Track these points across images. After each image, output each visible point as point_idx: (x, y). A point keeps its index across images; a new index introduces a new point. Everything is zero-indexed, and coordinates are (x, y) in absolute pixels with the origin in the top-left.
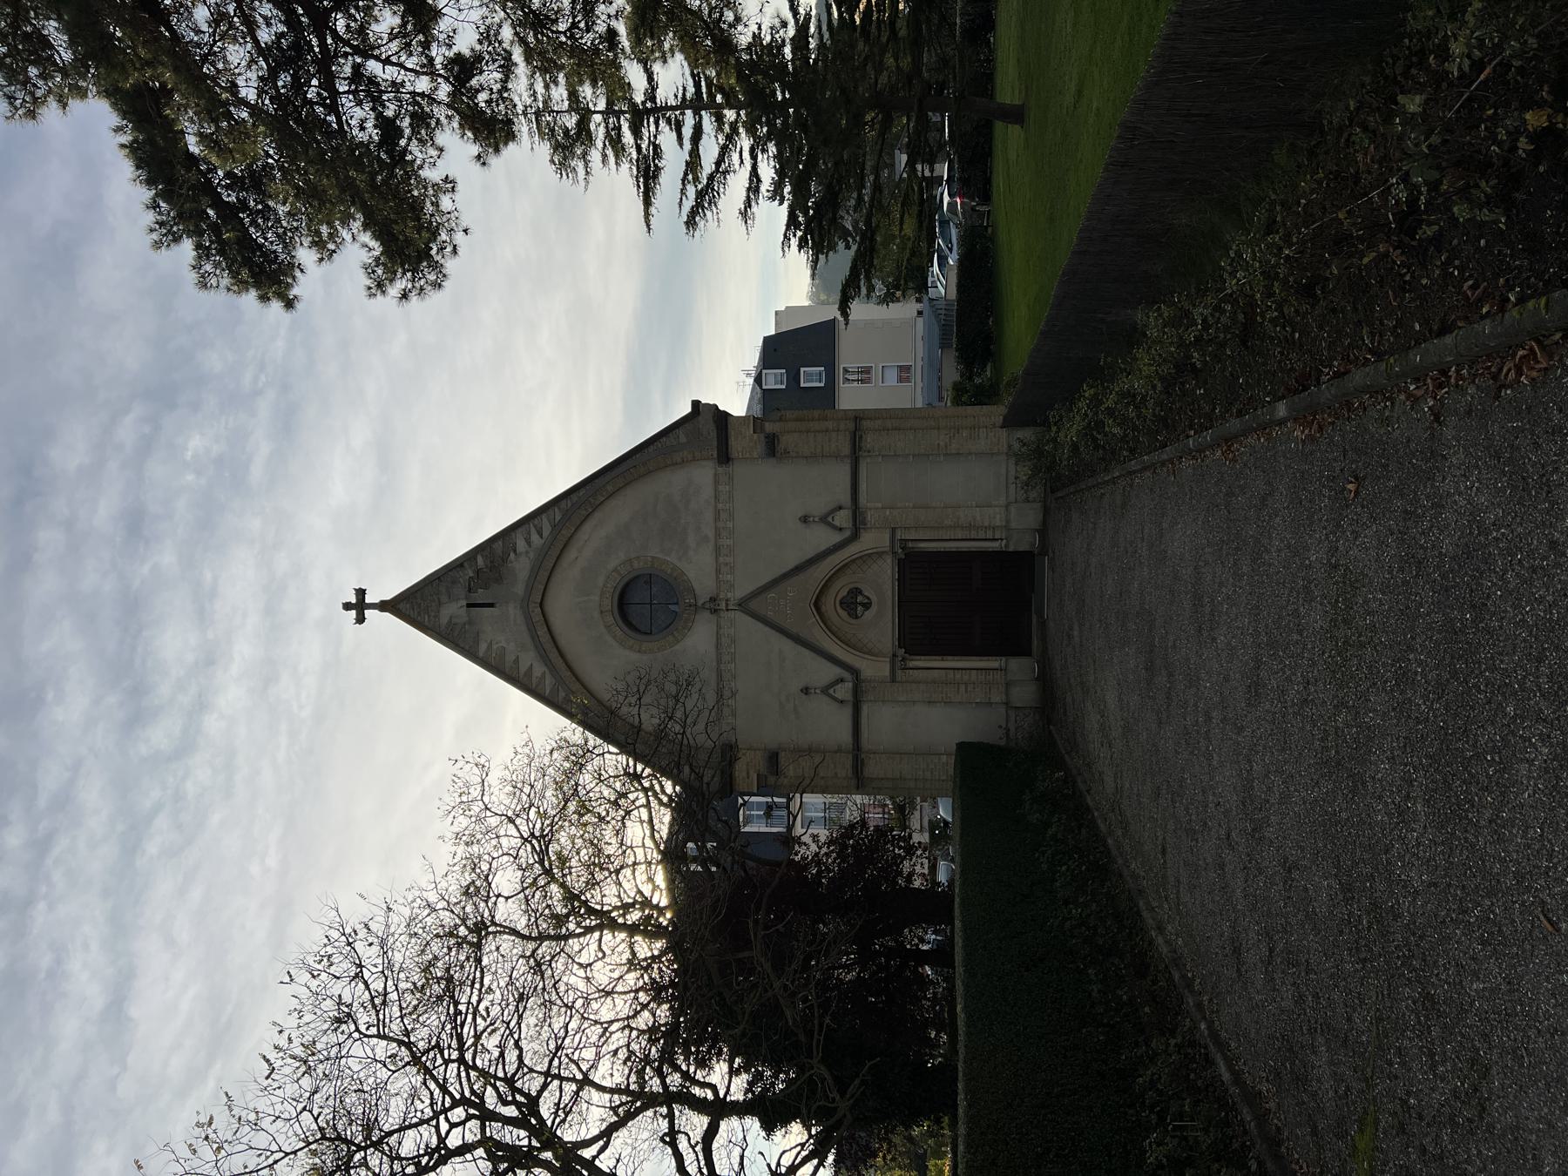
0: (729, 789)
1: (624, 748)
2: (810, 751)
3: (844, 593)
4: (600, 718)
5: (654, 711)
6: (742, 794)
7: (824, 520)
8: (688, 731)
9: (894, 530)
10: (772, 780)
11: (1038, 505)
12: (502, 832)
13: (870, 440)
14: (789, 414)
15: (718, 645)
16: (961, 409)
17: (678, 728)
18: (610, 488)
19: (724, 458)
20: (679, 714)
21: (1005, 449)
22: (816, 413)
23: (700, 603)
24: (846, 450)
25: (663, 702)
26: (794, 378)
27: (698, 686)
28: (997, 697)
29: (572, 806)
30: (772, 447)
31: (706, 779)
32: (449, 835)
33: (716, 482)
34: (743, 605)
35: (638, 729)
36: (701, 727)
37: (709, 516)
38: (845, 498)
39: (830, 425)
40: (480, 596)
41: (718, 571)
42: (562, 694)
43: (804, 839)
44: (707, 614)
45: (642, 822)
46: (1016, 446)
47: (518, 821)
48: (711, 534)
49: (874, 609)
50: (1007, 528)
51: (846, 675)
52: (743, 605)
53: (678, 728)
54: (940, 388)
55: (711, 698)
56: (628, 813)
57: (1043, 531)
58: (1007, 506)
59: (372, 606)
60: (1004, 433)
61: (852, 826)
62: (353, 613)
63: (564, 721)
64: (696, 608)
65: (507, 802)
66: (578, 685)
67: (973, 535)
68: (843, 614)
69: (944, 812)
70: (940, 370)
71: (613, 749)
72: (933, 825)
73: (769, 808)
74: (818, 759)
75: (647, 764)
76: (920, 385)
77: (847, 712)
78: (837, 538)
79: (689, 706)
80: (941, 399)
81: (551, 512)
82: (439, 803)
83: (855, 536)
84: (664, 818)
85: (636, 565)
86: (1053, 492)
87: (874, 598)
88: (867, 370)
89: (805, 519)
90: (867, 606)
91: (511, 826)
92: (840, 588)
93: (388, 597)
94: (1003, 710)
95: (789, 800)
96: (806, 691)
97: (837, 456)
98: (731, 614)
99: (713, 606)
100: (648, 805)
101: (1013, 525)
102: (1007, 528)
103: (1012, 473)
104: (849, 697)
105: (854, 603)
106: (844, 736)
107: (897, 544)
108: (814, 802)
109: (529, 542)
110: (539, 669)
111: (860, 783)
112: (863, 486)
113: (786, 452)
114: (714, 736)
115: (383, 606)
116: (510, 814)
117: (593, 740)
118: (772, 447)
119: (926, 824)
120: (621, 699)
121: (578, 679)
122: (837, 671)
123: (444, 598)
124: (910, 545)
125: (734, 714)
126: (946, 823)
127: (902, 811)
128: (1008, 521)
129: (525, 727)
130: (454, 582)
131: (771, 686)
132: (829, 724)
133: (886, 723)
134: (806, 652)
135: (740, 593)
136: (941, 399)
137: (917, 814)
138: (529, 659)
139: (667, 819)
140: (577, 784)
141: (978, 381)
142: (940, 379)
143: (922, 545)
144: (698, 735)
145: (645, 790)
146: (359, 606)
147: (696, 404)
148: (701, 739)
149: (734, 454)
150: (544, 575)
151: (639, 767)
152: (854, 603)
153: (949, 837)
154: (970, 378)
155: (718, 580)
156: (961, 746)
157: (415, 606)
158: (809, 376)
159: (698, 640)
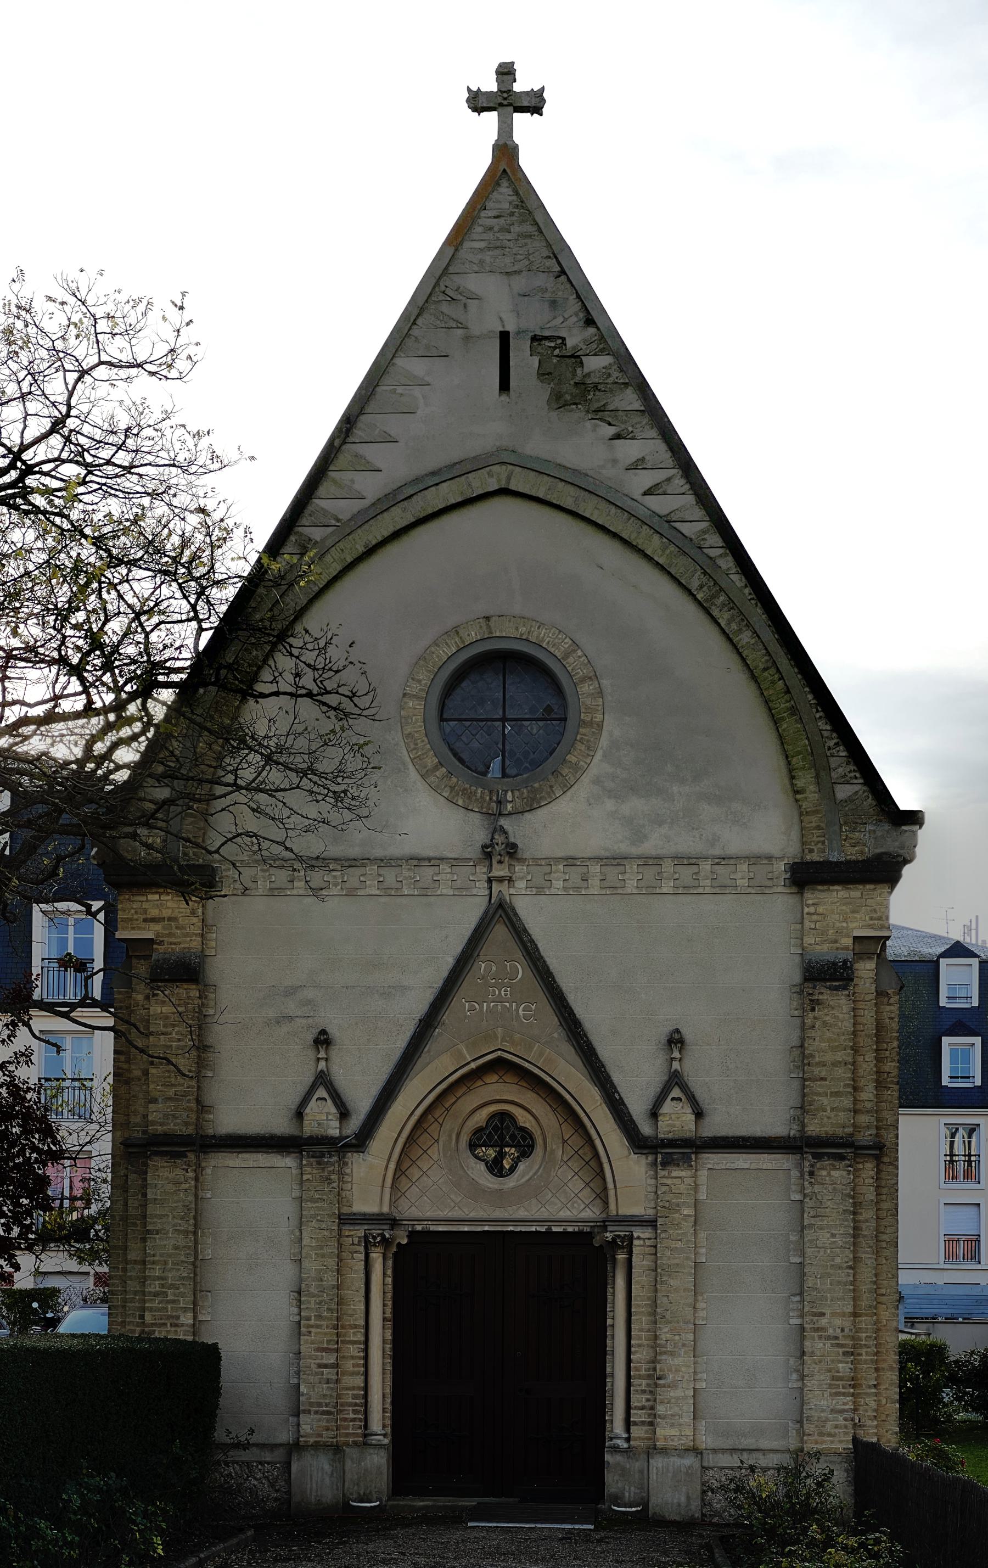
0: (123, 879)
1: (202, 660)
2: (202, 1049)
3: (524, 1120)
4: (259, 621)
5: (283, 726)
6: (110, 910)
7: (675, 1080)
8: (240, 797)
9: (652, 1223)
10: (141, 969)
11: (695, 1508)
12: (32, 407)
13: (835, 1175)
14: (892, 1009)
15: (418, 860)
16: (892, 1359)
17: (247, 774)
18: (745, 638)
19: (805, 876)
20: (275, 776)
21: (810, 1446)
22: (891, 1067)
23: (503, 822)
24: (814, 1128)
25: (301, 743)
26: (961, 1023)
27: (335, 817)
28: (309, 1425)
29: (87, 552)
30: (824, 976)
31: (142, 831)
32: (26, 292)
33: (754, 859)
34: (500, 913)
35: (247, 692)
36: (251, 823)
37: (686, 843)
38: (720, 1123)
39: (868, 1095)
40: (524, 362)
41: (570, 861)
42: (317, 534)
43: (22, 1031)
44: (481, 837)
45: (56, 698)
46: (817, 1469)
47: (56, 440)
48: (648, 848)
49: (489, 1181)
50: (652, 1450)
51: (354, 1124)
52: (500, 913)
53: (247, 774)
54: (932, 1320)
55: (311, 845)
56: (77, 671)
57: (646, 1521)
58: (696, 1451)
59: (506, 129)
60: (842, 1443)
61: (48, 1132)
62: (490, 85)
63: (262, 537)
64: (495, 814)
65: (96, 417)
66: (336, 568)
67: (640, 1384)
68: (481, 1117)
69: (81, 1320)
70: (968, 1320)
71: (206, 637)
72: (48, 1297)
73: (81, 966)
74: (184, 1063)
75: (174, 710)
76: (940, 1279)
77: (281, 1125)
78: (637, 1107)
79: (293, 798)
80: (911, 1321)
81: (699, 513)
82: (92, 272)
83: (638, 1142)
84: (64, 746)
85: (585, 688)
86: (724, 1540)
87: (510, 1182)
88: (972, 1172)
89: (675, 1041)
90: (495, 1167)
91: (47, 424)
92: (532, 1113)
93: (525, 162)
94: (284, 1436)
95: (103, 1005)
96: (323, 1040)
97: (803, 1108)
98: (481, 888)
99: (499, 851)
100: (89, 710)
101: (658, 1462)
102: (652, 1450)
103: (763, 1461)
104: (310, 1127)
105: (503, 1140)
106: (229, 1119)
107: (622, 1231)
108: (96, 1055)
109: (637, 465)
110: (371, 487)
111: (139, 1149)
112: (742, 1161)
113: (814, 1004)
114: (230, 850)
115: (505, 152)
116: (71, 423)
117: (224, 596)
118: (824, 976)
119: (50, 1283)
120: (309, 657)
121: (349, 567)
122: (362, 1104)
123: (520, 283)
124: (621, 1257)
125: (273, 892)
126: (55, 1322)
127: (74, 1235)
128: (664, 1451)
129: (245, 440)
130: (553, 304)
131: (331, 958)
132: (254, 1088)
133: (256, 1206)
134: (401, 1043)
135: (528, 909)
136: (911, 1321)
137: (72, 1265)
138: (389, 466)
139: (61, 752)
140: (134, 563)
141: (947, 1395)
142: (951, 1320)
143: (620, 1282)
144: (232, 817)
145: (118, 706)
146: (507, 99)
147: (914, 818)
148: (224, 824)
149: (811, 896)
150: (567, 497)
151: (167, 695)
152: (503, 1140)
153: (24, 1329)
154: (953, 1380)
155: (550, 861)
156: (211, 1354)
157: (505, 212)
158: (962, 1055)
159: (425, 816)
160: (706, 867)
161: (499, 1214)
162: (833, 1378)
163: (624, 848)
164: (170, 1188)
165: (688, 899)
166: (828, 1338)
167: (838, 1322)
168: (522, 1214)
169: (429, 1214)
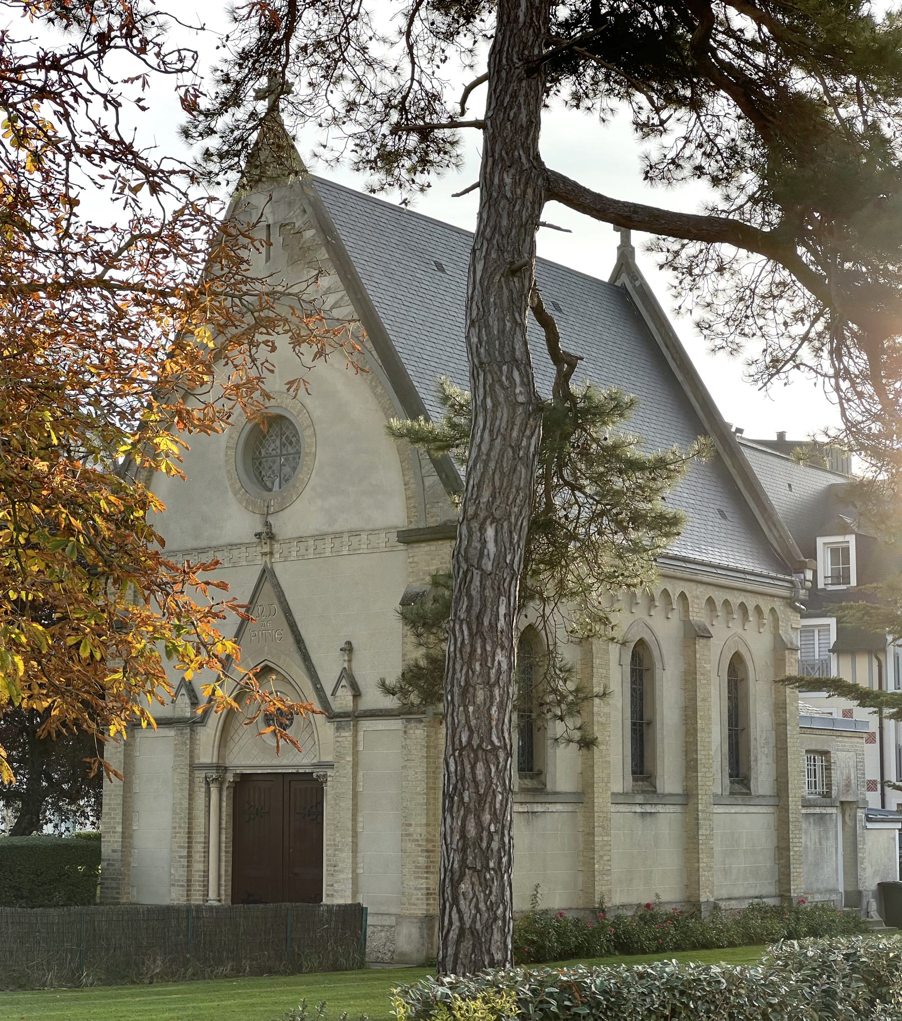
34: (267, 575)
37: (356, 523)
41: (300, 539)
48: (336, 528)
52: (267, 575)
135: (278, 569)
160: (364, 536)
161: (275, 762)
162: (416, 867)
163: (326, 529)
164: (113, 750)
165: (356, 557)
166: (414, 841)
167: (419, 830)
168: (285, 762)
169: (243, 763)
